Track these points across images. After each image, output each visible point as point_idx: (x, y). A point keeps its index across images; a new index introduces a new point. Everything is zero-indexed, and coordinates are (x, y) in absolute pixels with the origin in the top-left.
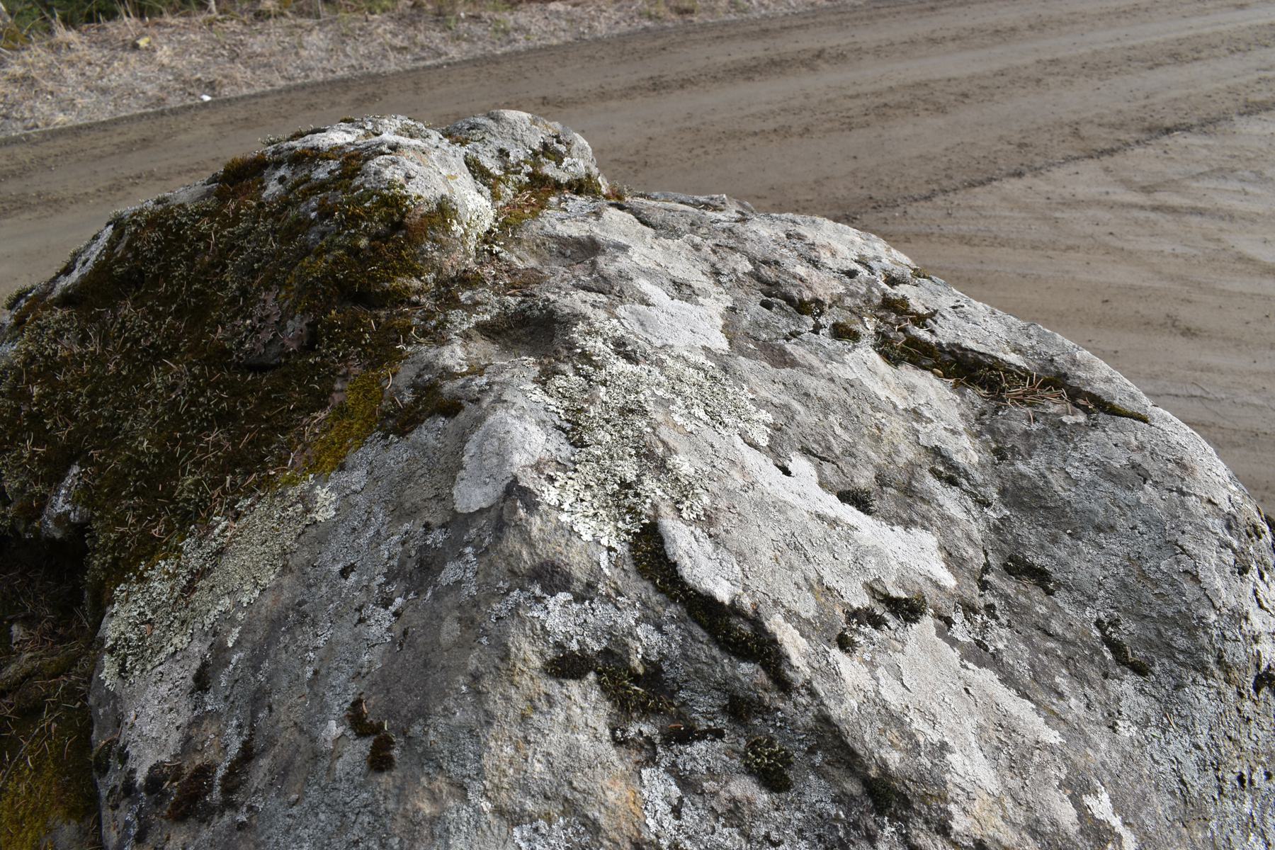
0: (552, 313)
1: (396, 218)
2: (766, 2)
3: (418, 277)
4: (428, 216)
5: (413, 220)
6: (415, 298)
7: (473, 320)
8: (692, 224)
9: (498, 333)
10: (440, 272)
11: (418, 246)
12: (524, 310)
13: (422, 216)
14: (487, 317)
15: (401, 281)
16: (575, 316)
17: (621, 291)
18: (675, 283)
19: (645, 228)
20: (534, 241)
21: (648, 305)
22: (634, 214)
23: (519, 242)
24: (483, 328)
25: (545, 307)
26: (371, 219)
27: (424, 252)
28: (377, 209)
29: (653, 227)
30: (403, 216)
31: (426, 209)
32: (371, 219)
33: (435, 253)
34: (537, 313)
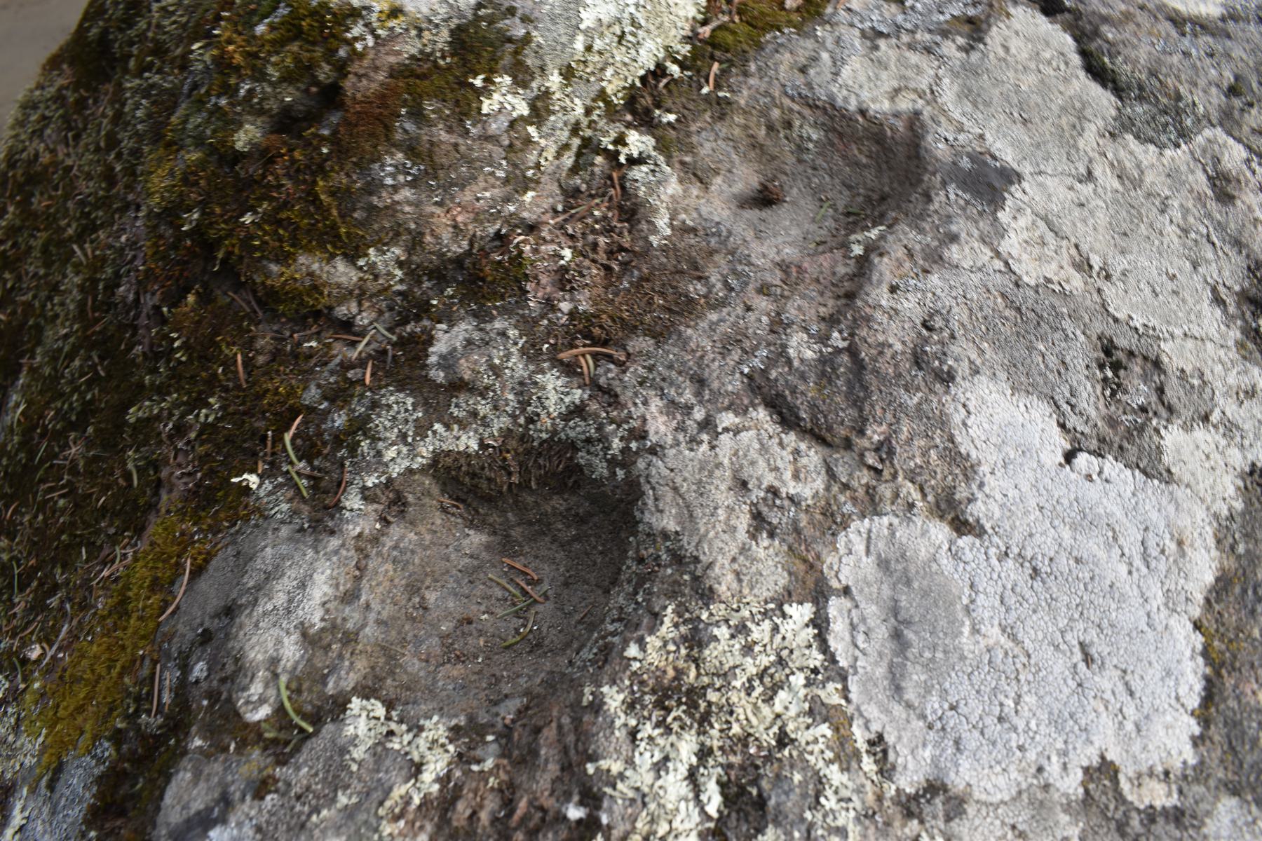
0: (633, 491)
1: (324, 72)
2: (642, 2)
3: (351, 259)
4: (415, 77)
5: (363, 85)
6: (342, 311)
7: (426, 450)
8: (1233, 91)
9: (489, 500)
10: (415, 243)
11: (362, 166)
12: (572, 446)
13: (394, 73)
14: (468, 442)
15: (309, 263)
16: (678, 559)
17: (885, 449)
18: (1108, 348)
19: (1095, 89)
20: (764, 113)
21: (961, 526)
22: (1081, 37)
23: (722, 109)
24: (451, 474)
25: (626, 460)
26: (260, 76)
27: (373, 187)
28: (278, 45)
29: (1118, 91)
30: (341, 68)
31: (410, 48)
32: (260, 76)
33: (406, 193)
34: (601, 469)
